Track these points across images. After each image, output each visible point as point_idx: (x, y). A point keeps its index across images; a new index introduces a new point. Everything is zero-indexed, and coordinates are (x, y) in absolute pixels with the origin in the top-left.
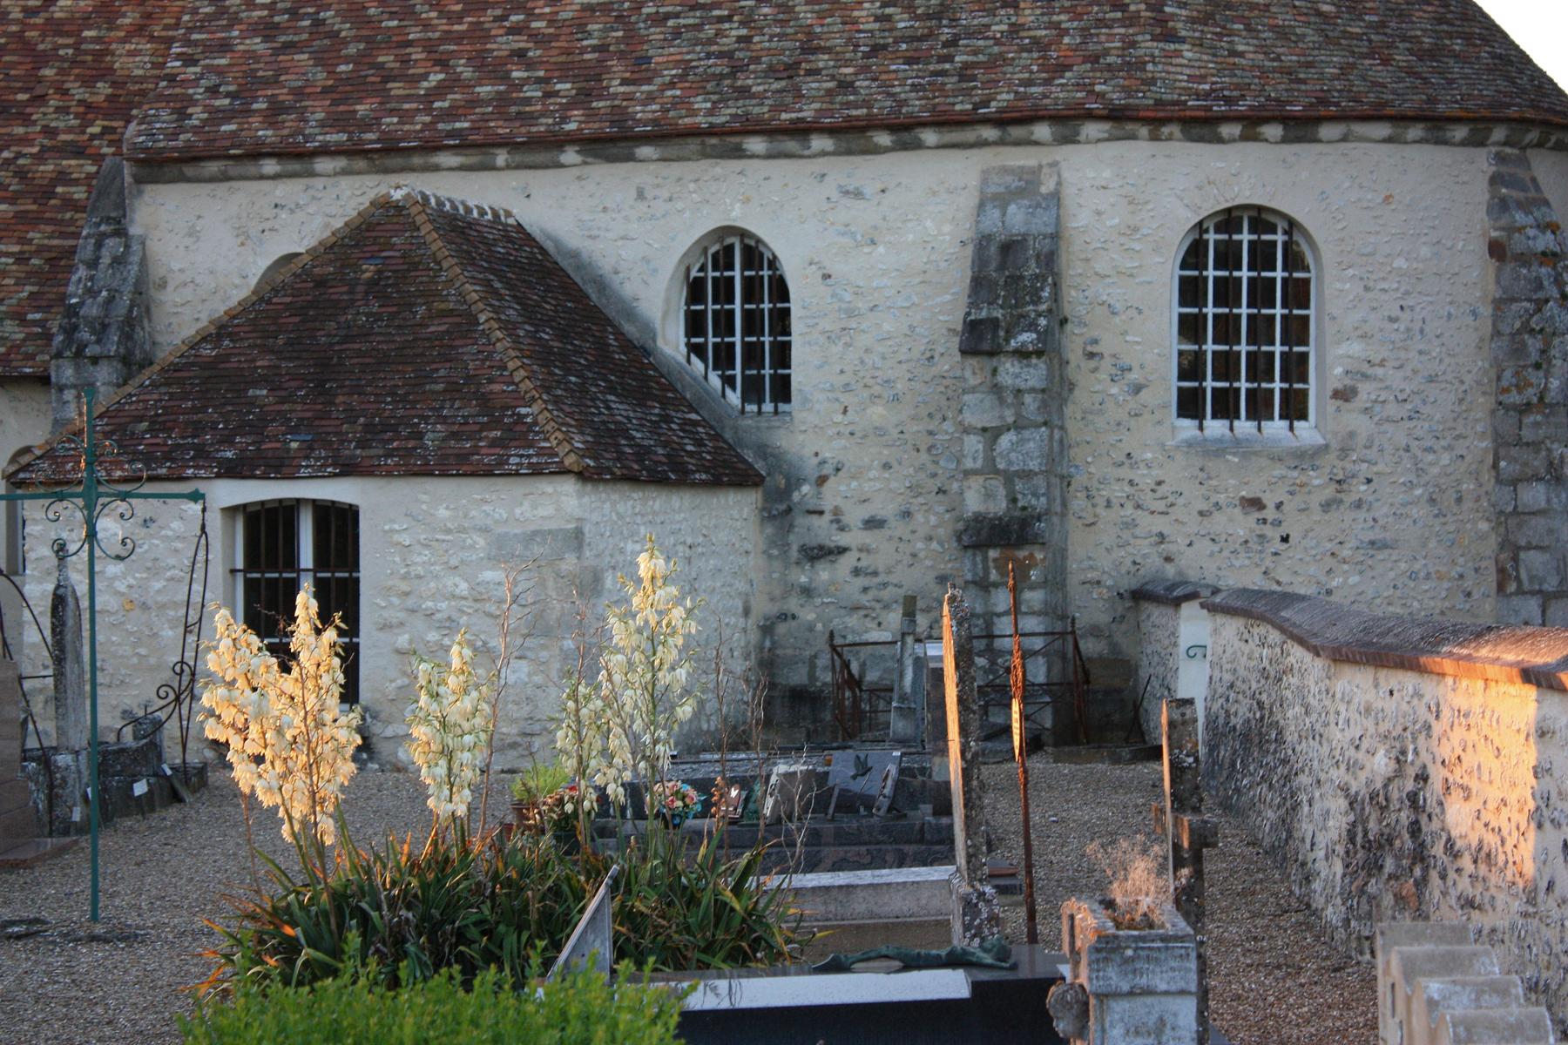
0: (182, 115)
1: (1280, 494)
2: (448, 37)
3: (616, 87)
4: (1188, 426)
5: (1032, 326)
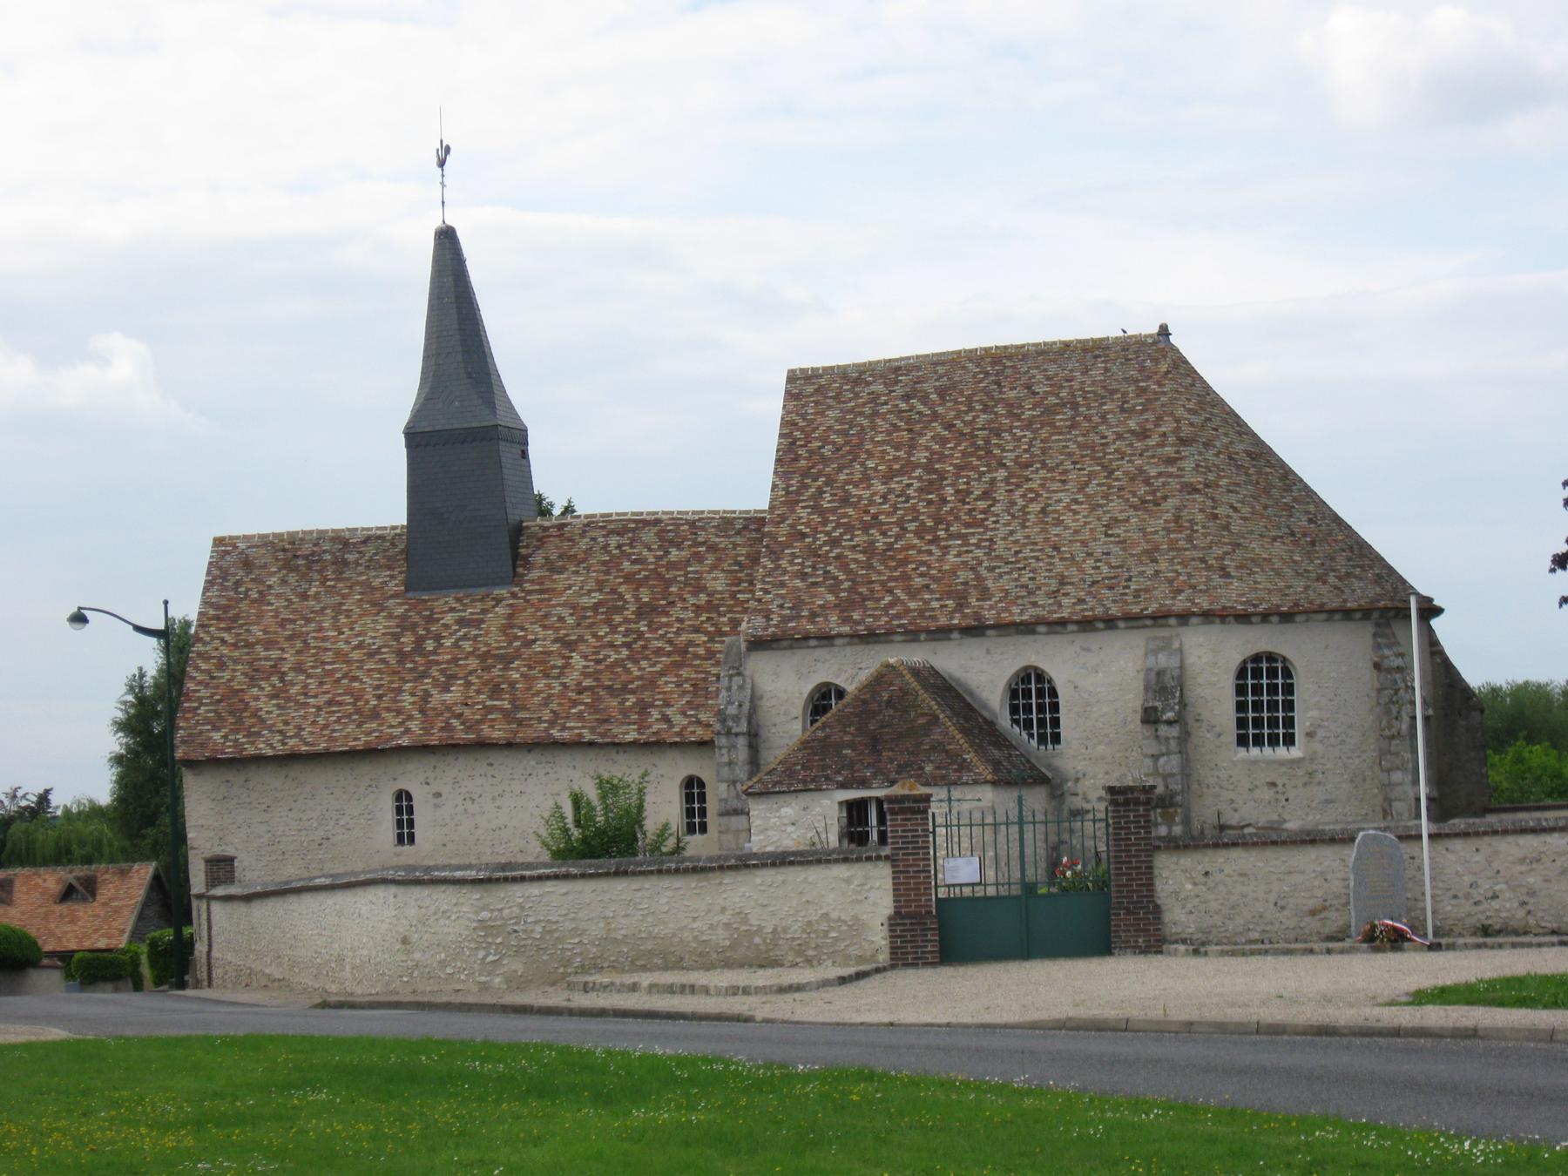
0: (768, 619)
1: (1284, 780)
2: (891, 579)
3: (973, 601)
4: (1242, 752)
5: (1172, 709)
